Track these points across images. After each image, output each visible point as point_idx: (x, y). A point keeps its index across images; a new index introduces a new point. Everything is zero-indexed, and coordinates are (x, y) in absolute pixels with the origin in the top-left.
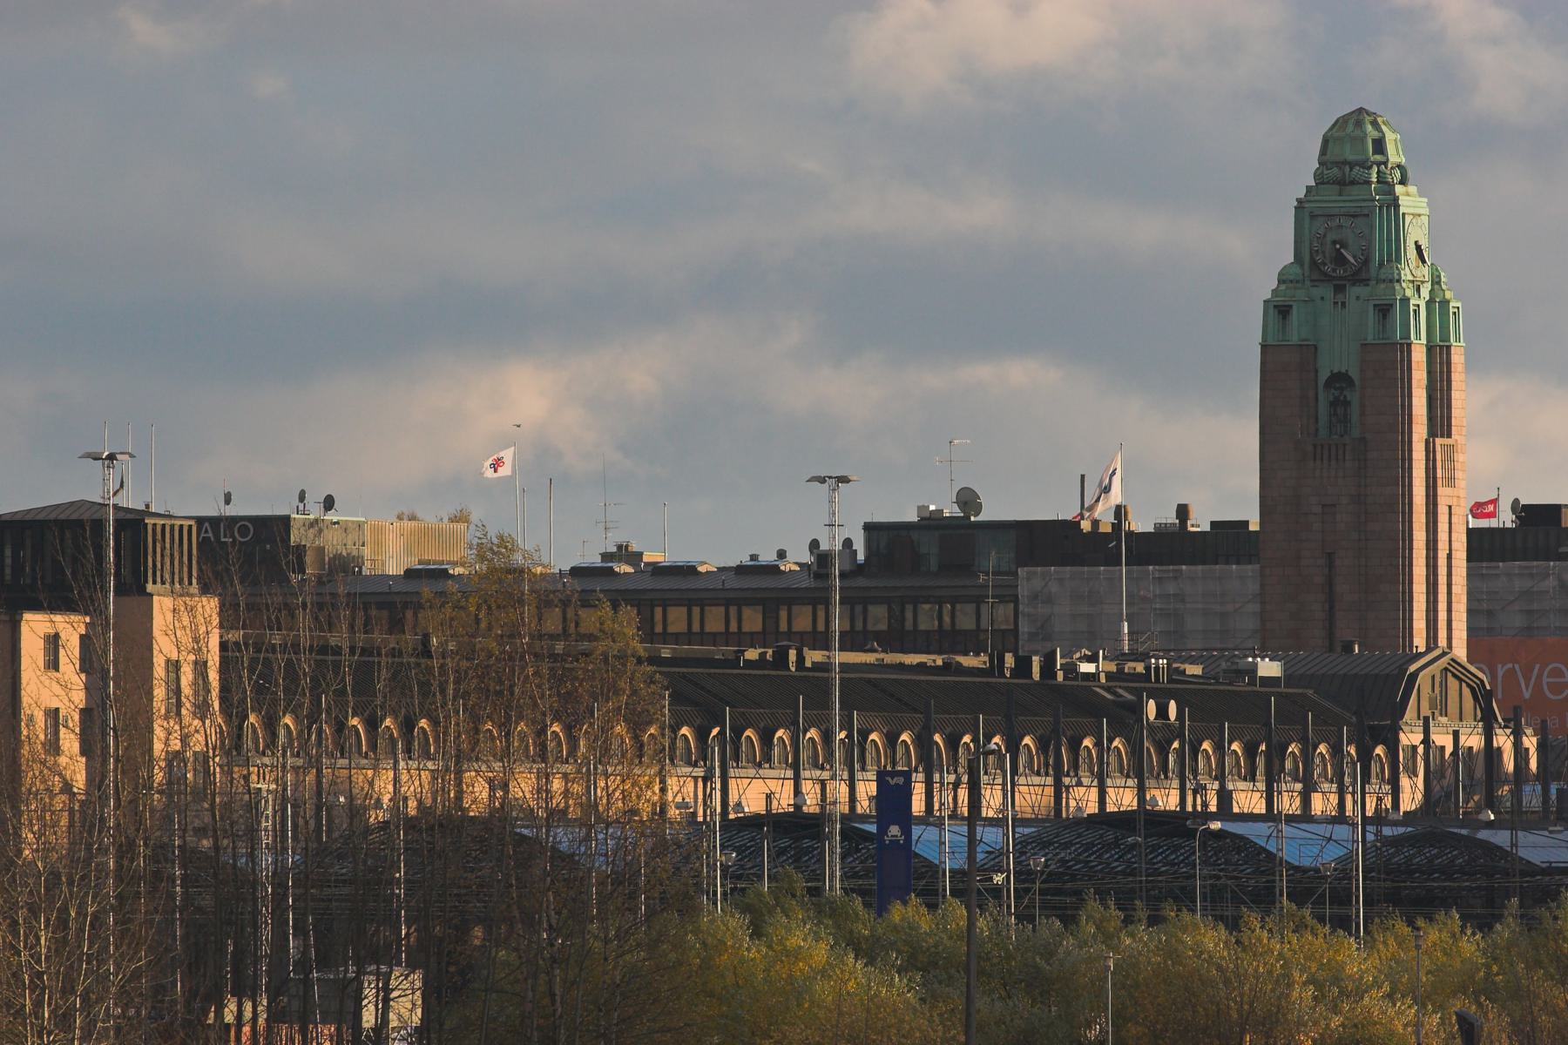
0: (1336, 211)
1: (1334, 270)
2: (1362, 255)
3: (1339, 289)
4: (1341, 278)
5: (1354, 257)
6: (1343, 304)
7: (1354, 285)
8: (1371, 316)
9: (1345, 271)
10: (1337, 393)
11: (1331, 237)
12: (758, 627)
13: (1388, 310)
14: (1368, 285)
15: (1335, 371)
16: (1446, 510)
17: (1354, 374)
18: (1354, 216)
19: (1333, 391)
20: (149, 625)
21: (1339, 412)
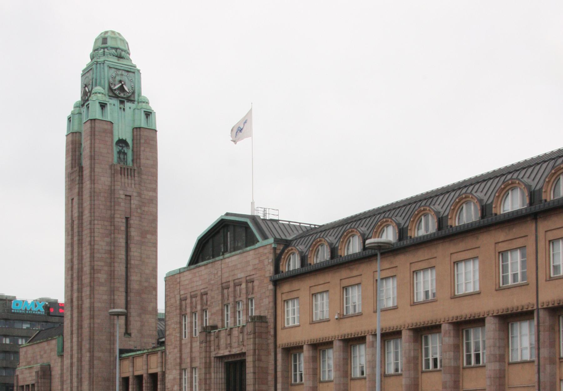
0: (120, 68)
1: (120, 94)
2: (132, 89)
3: (122, 102)
4: (122, 98)
5: (129, 90)
6: (124, 109)
7: (128, 102)
8: (143, 116)
9: (124, 95)
10: (120, 148)
11: (118, 78)
12: (51, 309)
13: (149, 115)
14: (134, 103)
15: (121, 138)
16: (357, 282)
17: (130, 141)
18: (128, 71)
19: (119, 147)
20: (152, 281)
21: (121, 157)
